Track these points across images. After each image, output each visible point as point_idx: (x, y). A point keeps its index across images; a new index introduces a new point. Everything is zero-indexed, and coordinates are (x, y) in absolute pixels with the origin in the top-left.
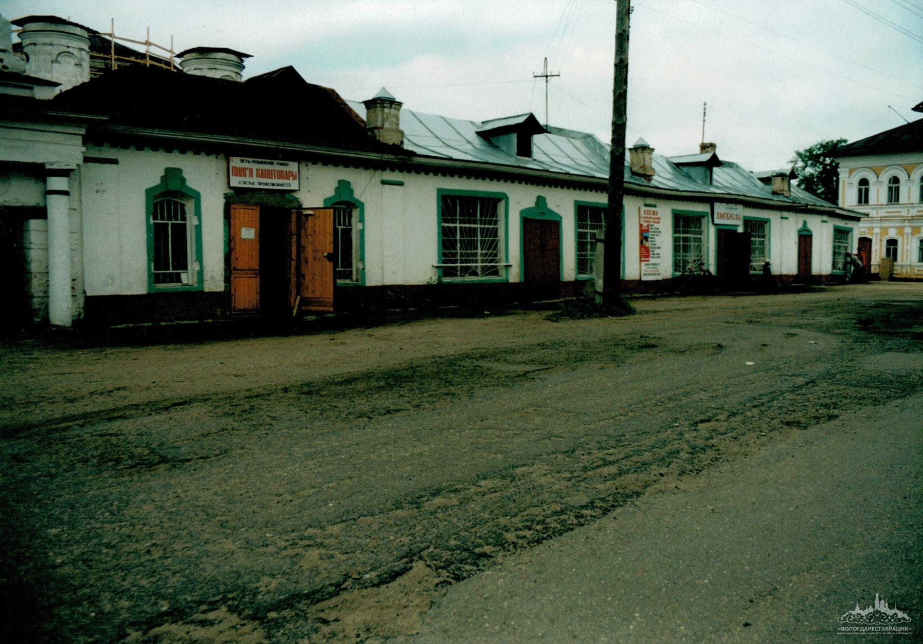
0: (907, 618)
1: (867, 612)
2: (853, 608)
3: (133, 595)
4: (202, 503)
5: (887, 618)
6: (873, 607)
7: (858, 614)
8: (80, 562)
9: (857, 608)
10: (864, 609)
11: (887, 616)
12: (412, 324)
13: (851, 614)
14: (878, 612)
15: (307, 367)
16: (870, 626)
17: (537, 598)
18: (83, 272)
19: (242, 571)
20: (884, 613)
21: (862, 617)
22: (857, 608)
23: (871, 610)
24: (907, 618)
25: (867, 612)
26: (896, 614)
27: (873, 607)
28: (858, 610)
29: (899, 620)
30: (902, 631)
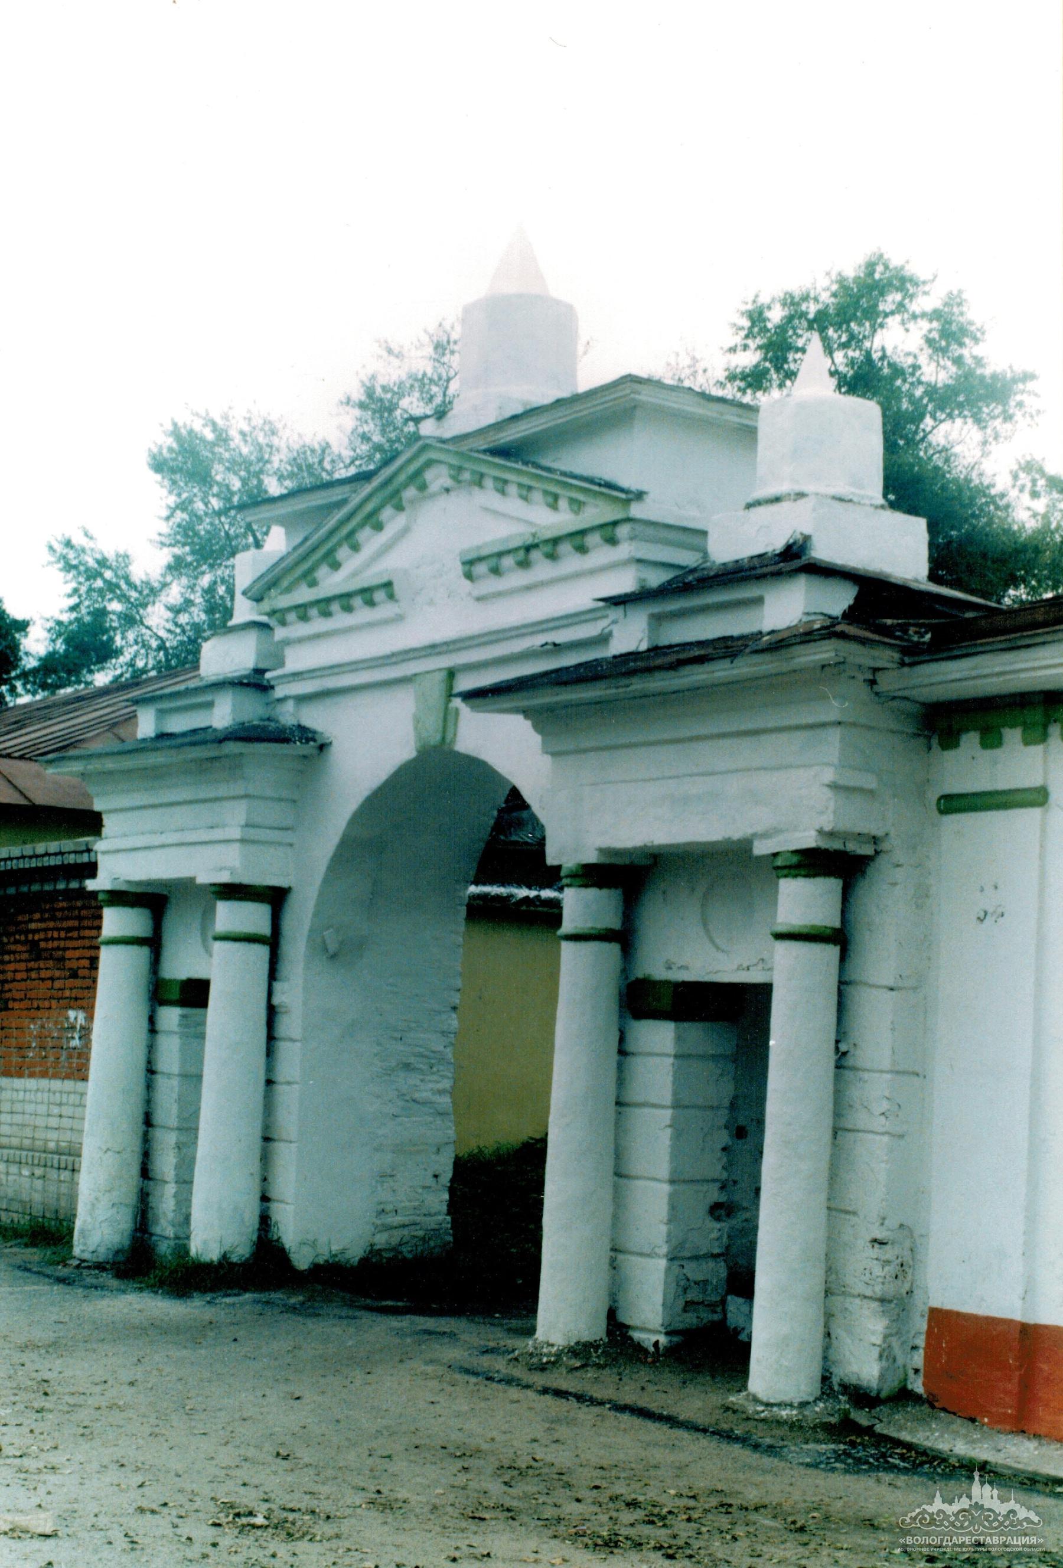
0: (1036, 1519)
1: (956, 1507)
2: (931, 1500)
3: (88, 579)
4: (43, 1299)
5: (996, 1519)
6: (970, 1497)
7: (940, 1511)
8: (34, 1045)
9: (938, 1499)
10: (951, 1502)
11: (997, 1515)
12: (155, 1147)
13: (925, 1511)
14: (978, 1506)
15: (39, 1172)
16: (962, 1534)
17: (324, 1425)
18: (825, 615)
19: (43, 1351)
20: (990, 1510)
21: (947, 1517)
22: (938, 1499)
23: (964, 1503)
24: (1036, 1519)
25: (956, 1507)
26: (1012, 1512)
27: (970, 1497)
28: (938, 1505)
29: (1020, 1523)
30: (1024, 1546)
